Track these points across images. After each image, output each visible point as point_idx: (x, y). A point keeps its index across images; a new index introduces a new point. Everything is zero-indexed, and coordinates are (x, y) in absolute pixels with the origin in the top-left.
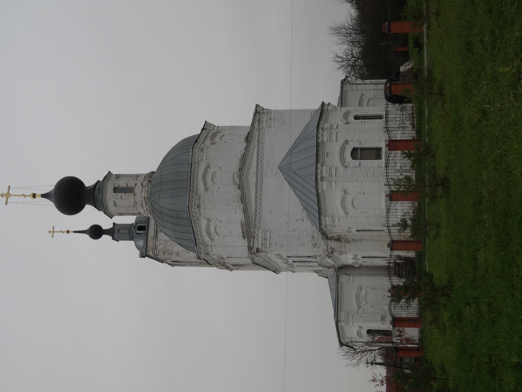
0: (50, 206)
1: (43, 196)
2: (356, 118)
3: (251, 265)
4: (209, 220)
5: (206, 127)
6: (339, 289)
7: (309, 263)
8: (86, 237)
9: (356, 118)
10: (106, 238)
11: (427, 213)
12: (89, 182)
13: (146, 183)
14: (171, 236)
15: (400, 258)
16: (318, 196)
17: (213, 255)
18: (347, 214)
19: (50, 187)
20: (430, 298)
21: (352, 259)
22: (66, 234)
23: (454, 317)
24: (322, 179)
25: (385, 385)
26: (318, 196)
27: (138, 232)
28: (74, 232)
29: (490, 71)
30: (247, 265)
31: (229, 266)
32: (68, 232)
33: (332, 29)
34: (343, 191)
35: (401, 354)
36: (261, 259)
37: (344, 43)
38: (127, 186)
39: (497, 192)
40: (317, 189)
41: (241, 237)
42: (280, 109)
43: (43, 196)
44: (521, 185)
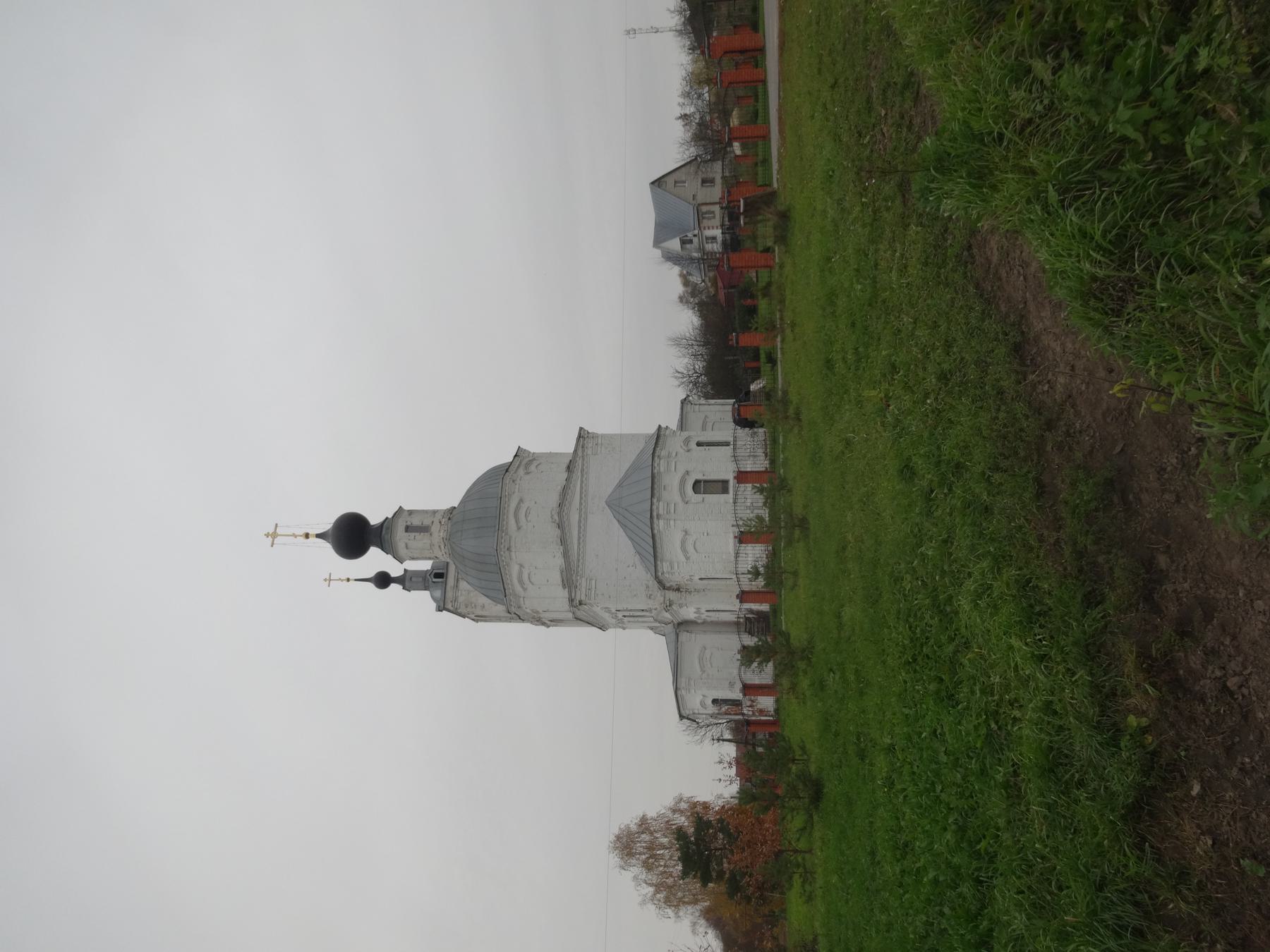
0: (327, 548)
1: (318, 536)
2: (699, 444)
4: (521, 566)
5: (519, 453)
8: (371, 586)
9: (699, 444)
10: (394, 587)
12: (374, 519)
16: (653, 536)
18: (687, 558)
19: (327, 524)
24: (658, 517)
26: (653, 536)
28: (356, 580)
32: (348, 580)
33: (670, 339)
37: (684, 356)
40: (652, 529)
41: (561, 587)
43: (318, 536)
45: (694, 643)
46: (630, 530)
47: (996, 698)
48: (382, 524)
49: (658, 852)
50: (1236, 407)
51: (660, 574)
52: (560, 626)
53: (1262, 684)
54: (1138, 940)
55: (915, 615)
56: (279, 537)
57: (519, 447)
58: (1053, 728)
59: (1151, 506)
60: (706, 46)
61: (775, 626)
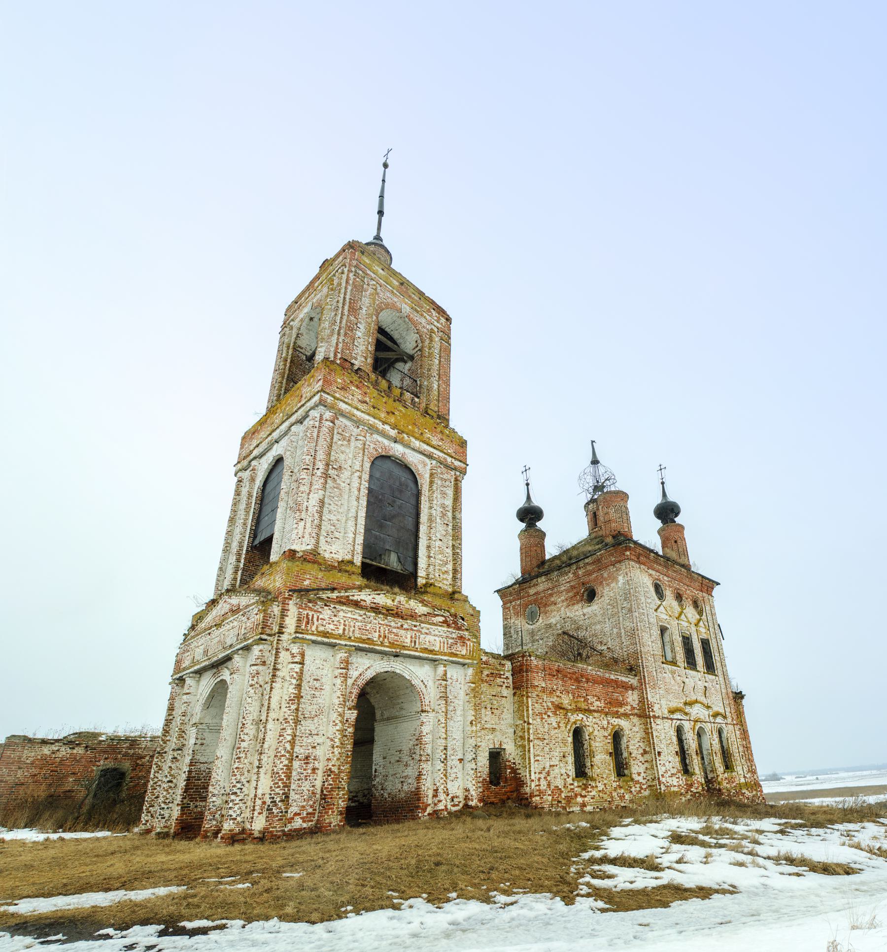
0: (659, 500)
2: (578, 734)
3: (725, 675)
5: (708, 585)
6: (460, 667)
7: (276, 498)
9: (578, 734)
11: (47, 840)
13: (365, 601)
14: (270, 434)
15: (597, 848)
17: (631, 883)
20: (60, 830)
21: (288, 610)
22: (384, 160)
23: (485, 887)
25: (400, 571)
27: (668, 626)
29: (255, 912)
30: (717, 891)
31: (485, 907)
32: (386, 166)
34: (624, 775)
35: (299, 397)
36: (680, 717)
38: (227, 667)
39: (277, 603)
42: (519, 554)
44: (14, 896)
45: (446, 585)
46: (768, 832)
47: (368, 875)
48: (594, 519)
49: (174, 889)
50: (679, 731)
51: (195, 644)
52: (444, 376)
53: (453, 623)
54: (49, 938)
55: (279, 776)
56: (381, 235)
57: (718, 584)
58: (537, 786)
59: (408, 396)
60: (530, 709)
61: (477, 942)
